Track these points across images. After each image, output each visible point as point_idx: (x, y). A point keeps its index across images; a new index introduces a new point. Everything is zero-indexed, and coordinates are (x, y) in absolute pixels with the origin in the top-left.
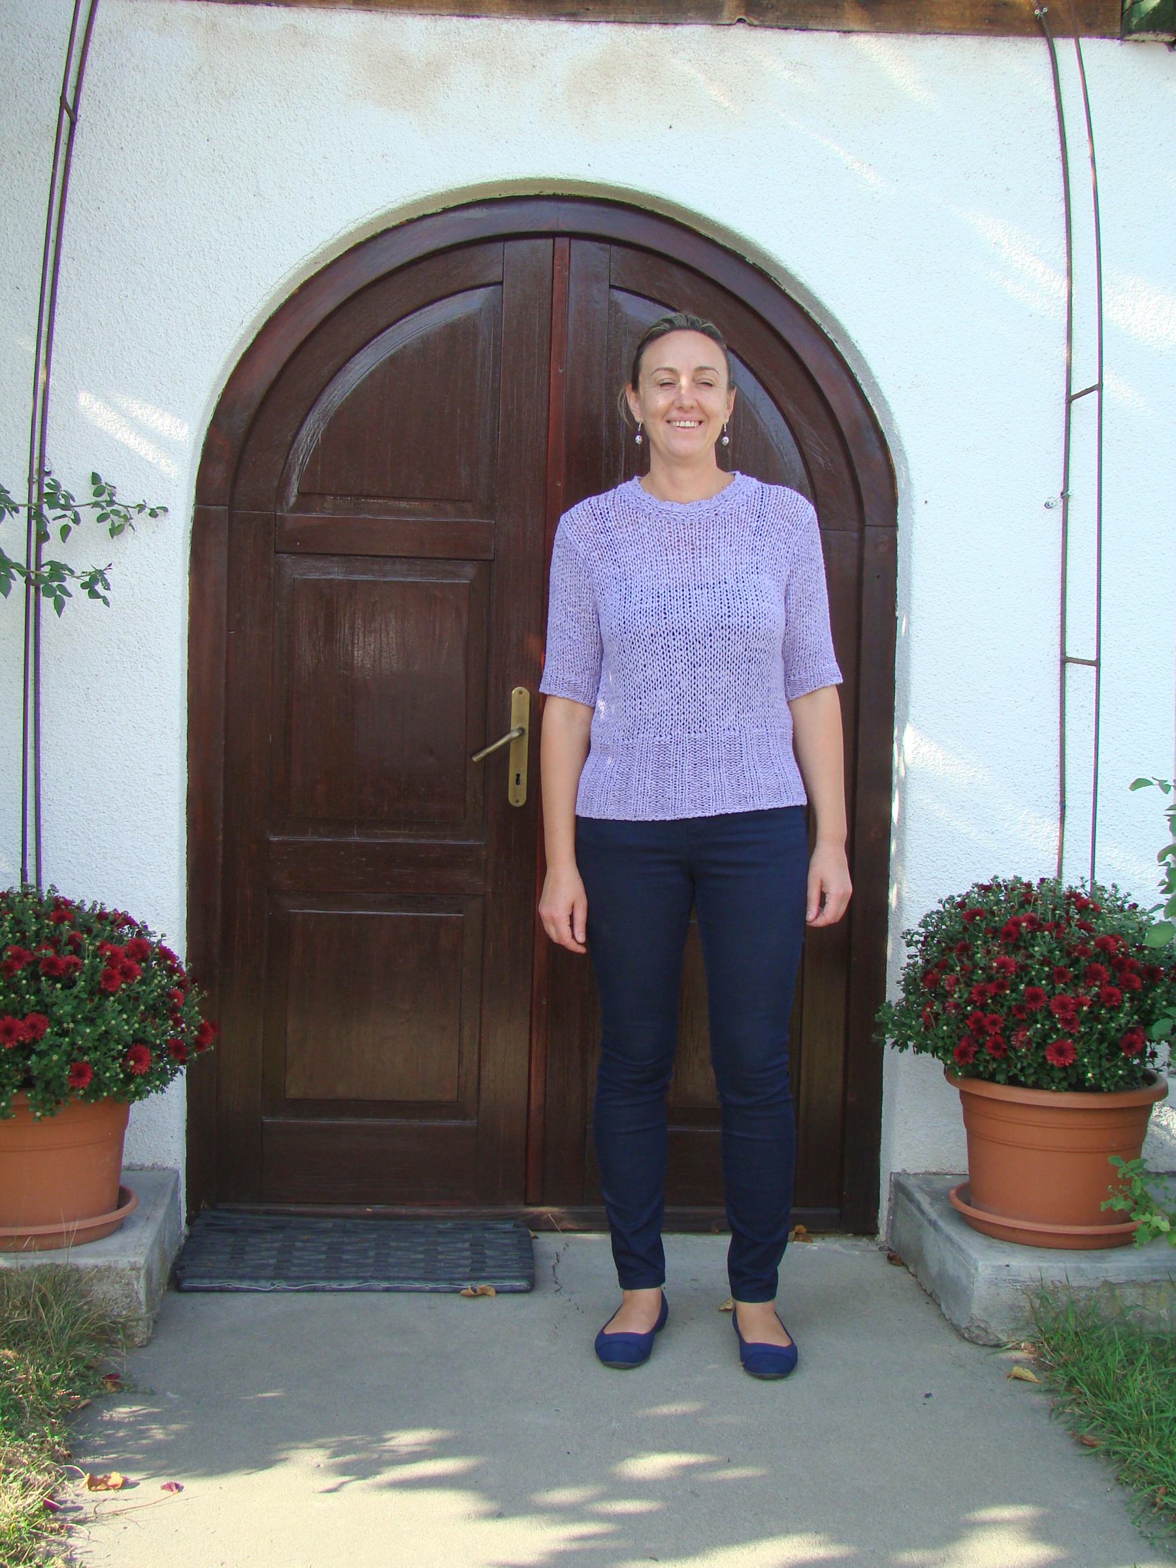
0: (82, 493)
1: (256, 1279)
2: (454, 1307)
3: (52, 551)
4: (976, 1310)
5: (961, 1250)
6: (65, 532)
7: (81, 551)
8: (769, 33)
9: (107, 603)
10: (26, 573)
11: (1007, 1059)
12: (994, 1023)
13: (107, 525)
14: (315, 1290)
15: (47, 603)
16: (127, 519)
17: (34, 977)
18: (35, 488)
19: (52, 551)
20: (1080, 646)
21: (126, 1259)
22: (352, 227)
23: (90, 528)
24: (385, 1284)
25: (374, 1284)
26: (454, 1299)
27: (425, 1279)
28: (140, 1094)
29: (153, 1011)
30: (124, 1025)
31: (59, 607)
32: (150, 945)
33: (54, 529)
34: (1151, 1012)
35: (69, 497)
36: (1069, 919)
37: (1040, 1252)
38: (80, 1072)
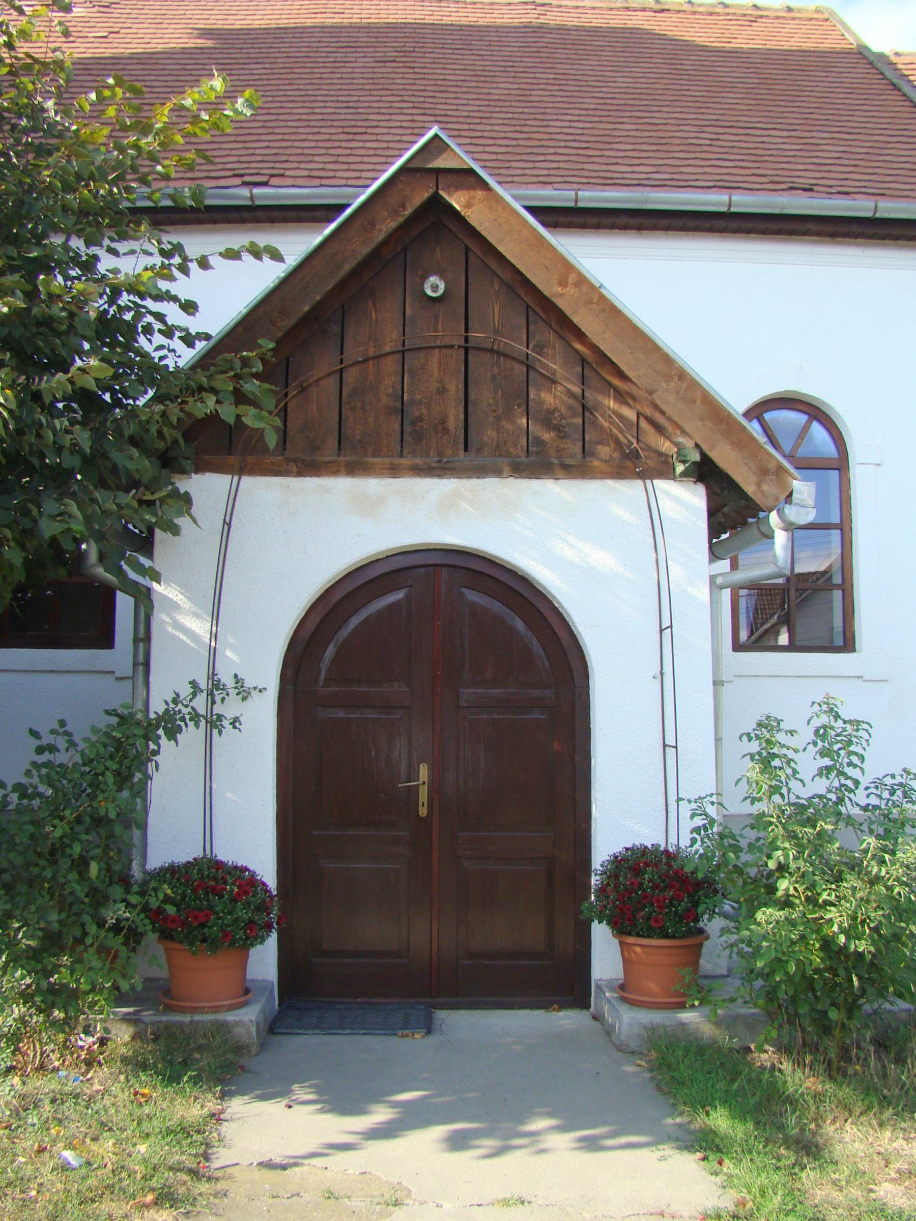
0: (229, 682)
1: (306, 1029)
2: (393, 1041)
3: (218, 709)
4: (623, 1037)
5: (617, 1011)
6: (223, 699)
7: (229, 708)
8: (523, 481)
9: (240, 730)
10: (205, 718)
11: (635, 925)
12: (629, 909)
13: (241, 696)
14: (333, 1034)
15: (215, 731)
16: (249, 693)
17: (207, 894)
18: (210, 681)
19: (218, 709)
20: (670, 741)
21: (247, 1018)
22: (346, 566)
23: (233, 698)
24: (363, 1031)
25: (358, 1031)
26: (395, 1038)
27: (381, 1029)
28: (252, 945)
29: (258, 909)
30: (243, 914)
31: (220, 733)
32: (257, 880)
33: (218, 699)
34: (698, 901)
35: (224, 685)
36: (661, 861)
37: (653, 1011)
38: (226, 935)
